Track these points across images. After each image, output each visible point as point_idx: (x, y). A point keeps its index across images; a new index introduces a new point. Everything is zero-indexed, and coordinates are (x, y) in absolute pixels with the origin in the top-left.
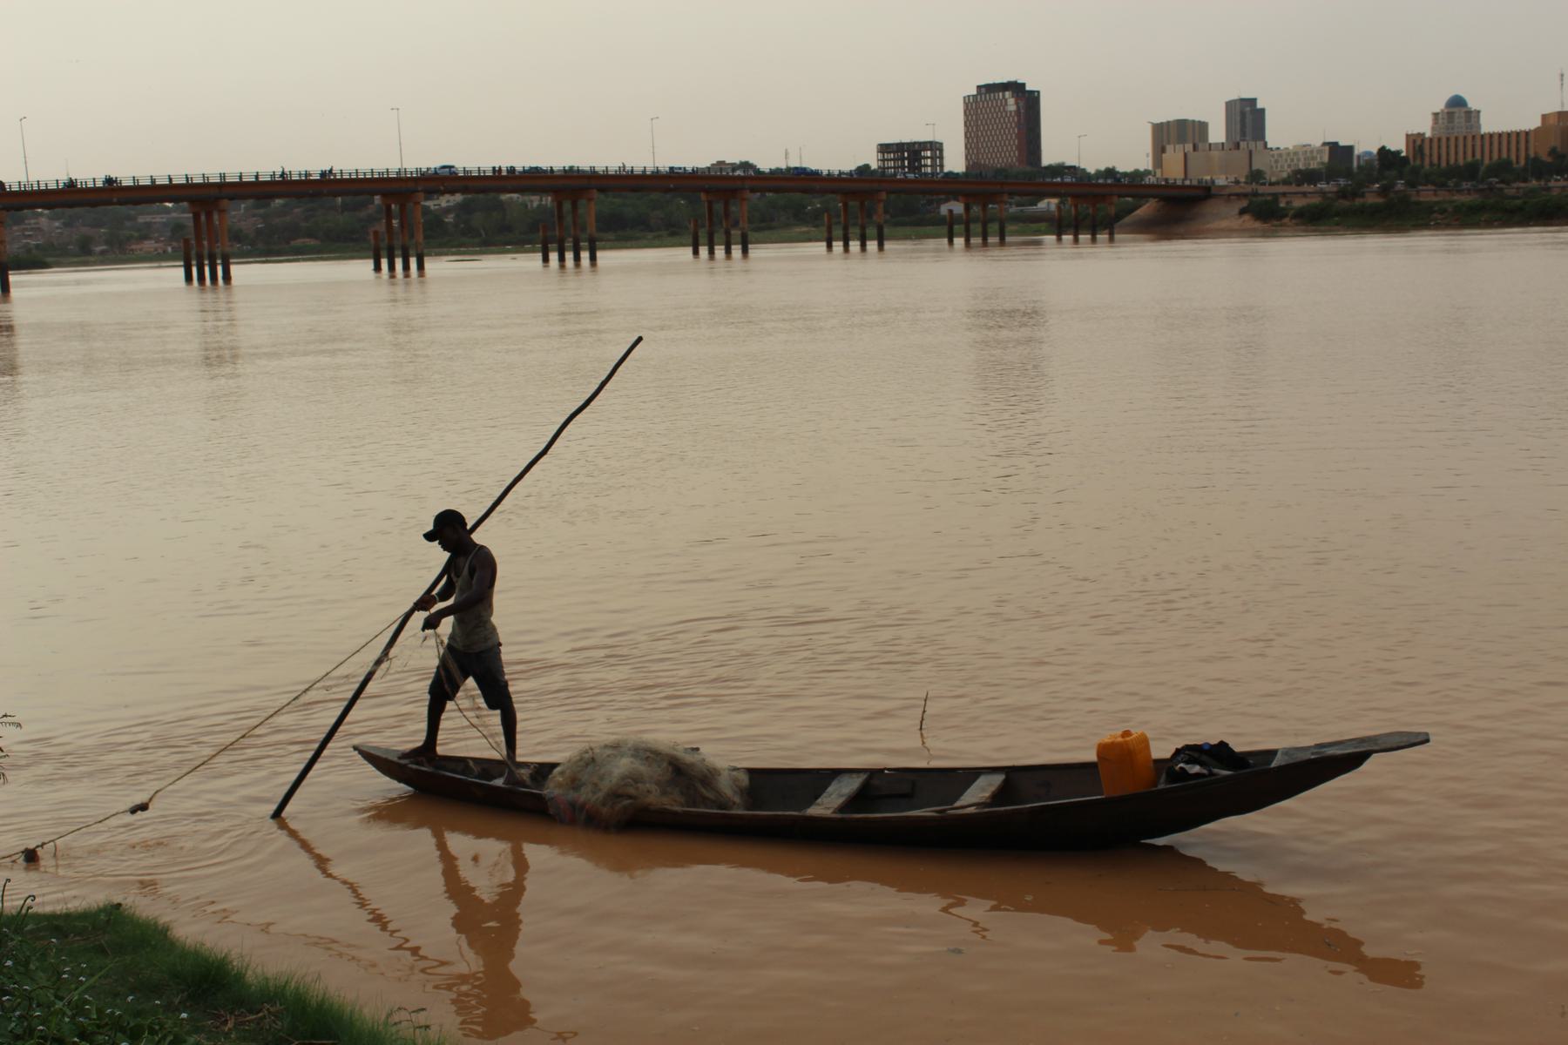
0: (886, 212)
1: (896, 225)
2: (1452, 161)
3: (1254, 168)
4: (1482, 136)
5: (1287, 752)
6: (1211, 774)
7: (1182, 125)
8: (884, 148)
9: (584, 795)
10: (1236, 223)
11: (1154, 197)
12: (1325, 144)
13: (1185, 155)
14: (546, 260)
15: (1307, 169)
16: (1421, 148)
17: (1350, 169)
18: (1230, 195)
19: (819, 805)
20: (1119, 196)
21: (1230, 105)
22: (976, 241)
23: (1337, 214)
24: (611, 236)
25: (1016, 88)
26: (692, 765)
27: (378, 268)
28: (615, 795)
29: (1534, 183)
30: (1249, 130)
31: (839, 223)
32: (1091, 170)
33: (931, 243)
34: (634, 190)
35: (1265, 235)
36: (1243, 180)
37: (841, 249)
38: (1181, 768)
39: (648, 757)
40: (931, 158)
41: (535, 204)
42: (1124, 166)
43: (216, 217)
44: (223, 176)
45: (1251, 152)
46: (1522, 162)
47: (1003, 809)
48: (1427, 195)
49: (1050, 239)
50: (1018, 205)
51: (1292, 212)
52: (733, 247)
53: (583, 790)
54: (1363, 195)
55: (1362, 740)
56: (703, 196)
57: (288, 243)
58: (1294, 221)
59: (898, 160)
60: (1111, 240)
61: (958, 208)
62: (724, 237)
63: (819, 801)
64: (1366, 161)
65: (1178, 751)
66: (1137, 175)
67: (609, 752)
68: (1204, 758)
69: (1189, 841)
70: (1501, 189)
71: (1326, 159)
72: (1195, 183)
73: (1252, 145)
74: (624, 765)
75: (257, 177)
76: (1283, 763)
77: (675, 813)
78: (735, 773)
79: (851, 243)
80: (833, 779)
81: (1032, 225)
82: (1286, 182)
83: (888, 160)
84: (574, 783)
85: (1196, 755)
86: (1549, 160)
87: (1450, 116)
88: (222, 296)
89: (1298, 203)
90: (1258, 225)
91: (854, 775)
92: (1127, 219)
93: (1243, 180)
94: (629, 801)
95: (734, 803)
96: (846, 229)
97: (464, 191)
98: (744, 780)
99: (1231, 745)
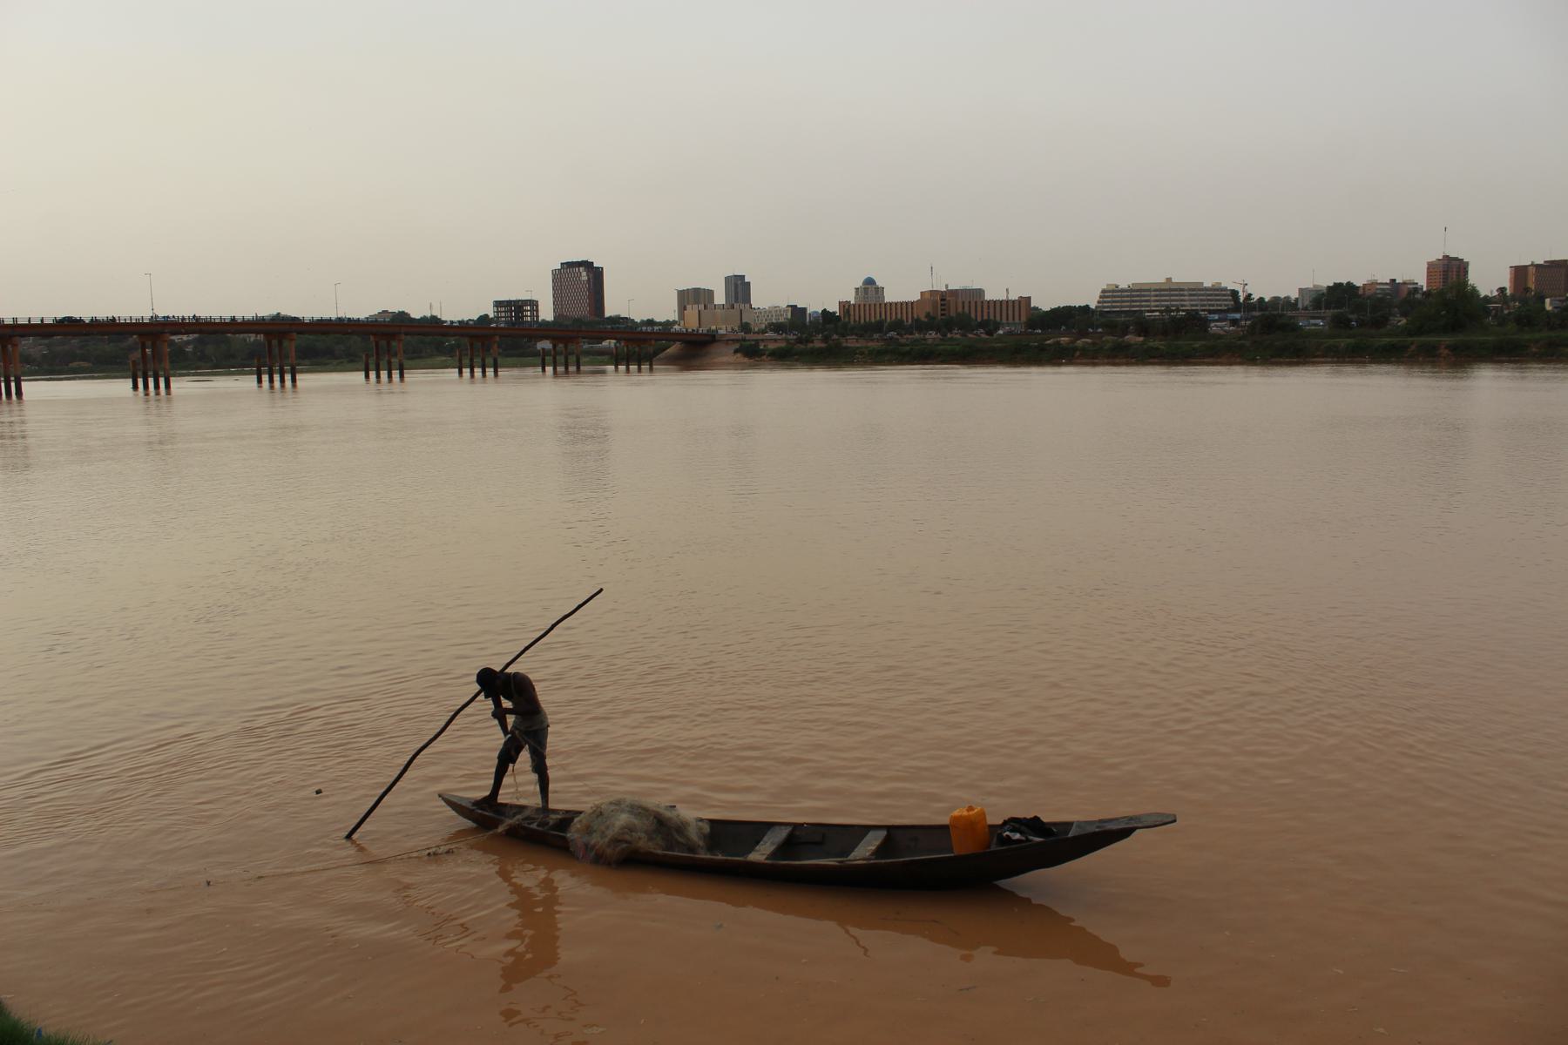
0: (499, 347)
1: (507, 356)
2: (868, 320)
3: (744, 321)
4: (885, 304)
5: (1080, 824)
6: (1028, 840)
7: (697, 291)
8: (498, 304)
9: (595, 839)
10: (732, 359)
11: (679, 341)
12: (788, 306)
13: (699, 312)
14: (260, 381)
15: (777, 323)
16: (848, 311)
17: (804, 324)
18: (728, 340)
19: (757, 851)
20: (656, 340)
21: (728, 279)
22: (561, 369)
23: (796, 354)
24: (307, 362)
25: (587, 265)
26: (670, 819)
27: (135, 387)
28: (616, 841)
29: (917, 336)
30: (740, 295)
31: (467, 355)
32: (638, 320)
33: (530, 371)
34: (324, 333)
35: (743, 367)
36: (736, 328)
37: (480, 374)
38: (1007, 835)
39: (640, 813)
40: (530, 311)
41: (252, 339)
42: (660, 318)
43: (10, 348)
44: (15, 319)
45: (741, 311)
46: (910, 321)
47: (883, 861)
48: (852, 342)
49: (611, 368)
50: (589, 344)
51: (767, 353)
52: (393, 372)
53: (594, 834)
54: (812, 342)
55: (1131, 819)
56: (372, 338)
57: (67, 365)
58: (769, 358)
59: (507, 312)
60: (651, 370)
61: (545, 345)
62: (386, 366)
63: (757, 848)
64: (814, 318)
65: (1005, 823)
66: (668, 324)
67: (613, 807)
68: (1023, 828)
69: (1004, 883)
70: (897, 339)
71: (789, 316)
72: (705, 332)
73: (742, 306)
74: (623, 819)
75: (42, 320)
76: (1077, 834)
77: (657, 855)
78: (700, 824)
79: (476, 370)
80: (769, 829)
81: (599, 357)
82: (764, 332)
83: (501, 312)
84: (589, 830)
85: (1017, 826)
86: (926, 320)
87: (866, 290)
88: (15, 407)
89: (772, 346)
90: (746, 360)
91: (783, 827)
92: (662, 355)
93: (736, 328)
94: (624, 845)
95: (699, 846)
96: (472, 360)
97: (200, 332)
98: (707, 828)
99: (1042, 818)
